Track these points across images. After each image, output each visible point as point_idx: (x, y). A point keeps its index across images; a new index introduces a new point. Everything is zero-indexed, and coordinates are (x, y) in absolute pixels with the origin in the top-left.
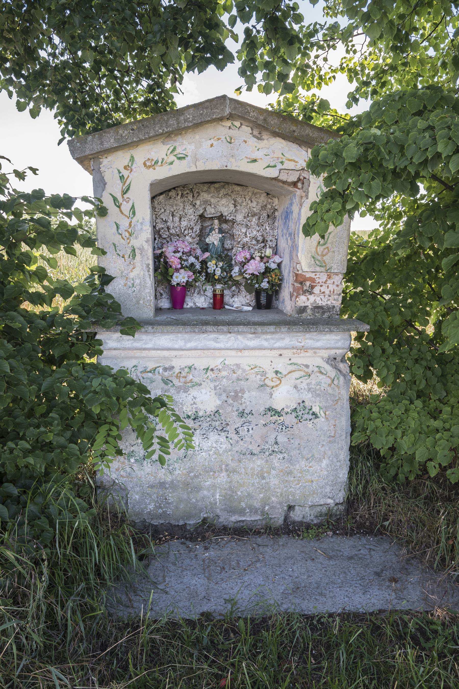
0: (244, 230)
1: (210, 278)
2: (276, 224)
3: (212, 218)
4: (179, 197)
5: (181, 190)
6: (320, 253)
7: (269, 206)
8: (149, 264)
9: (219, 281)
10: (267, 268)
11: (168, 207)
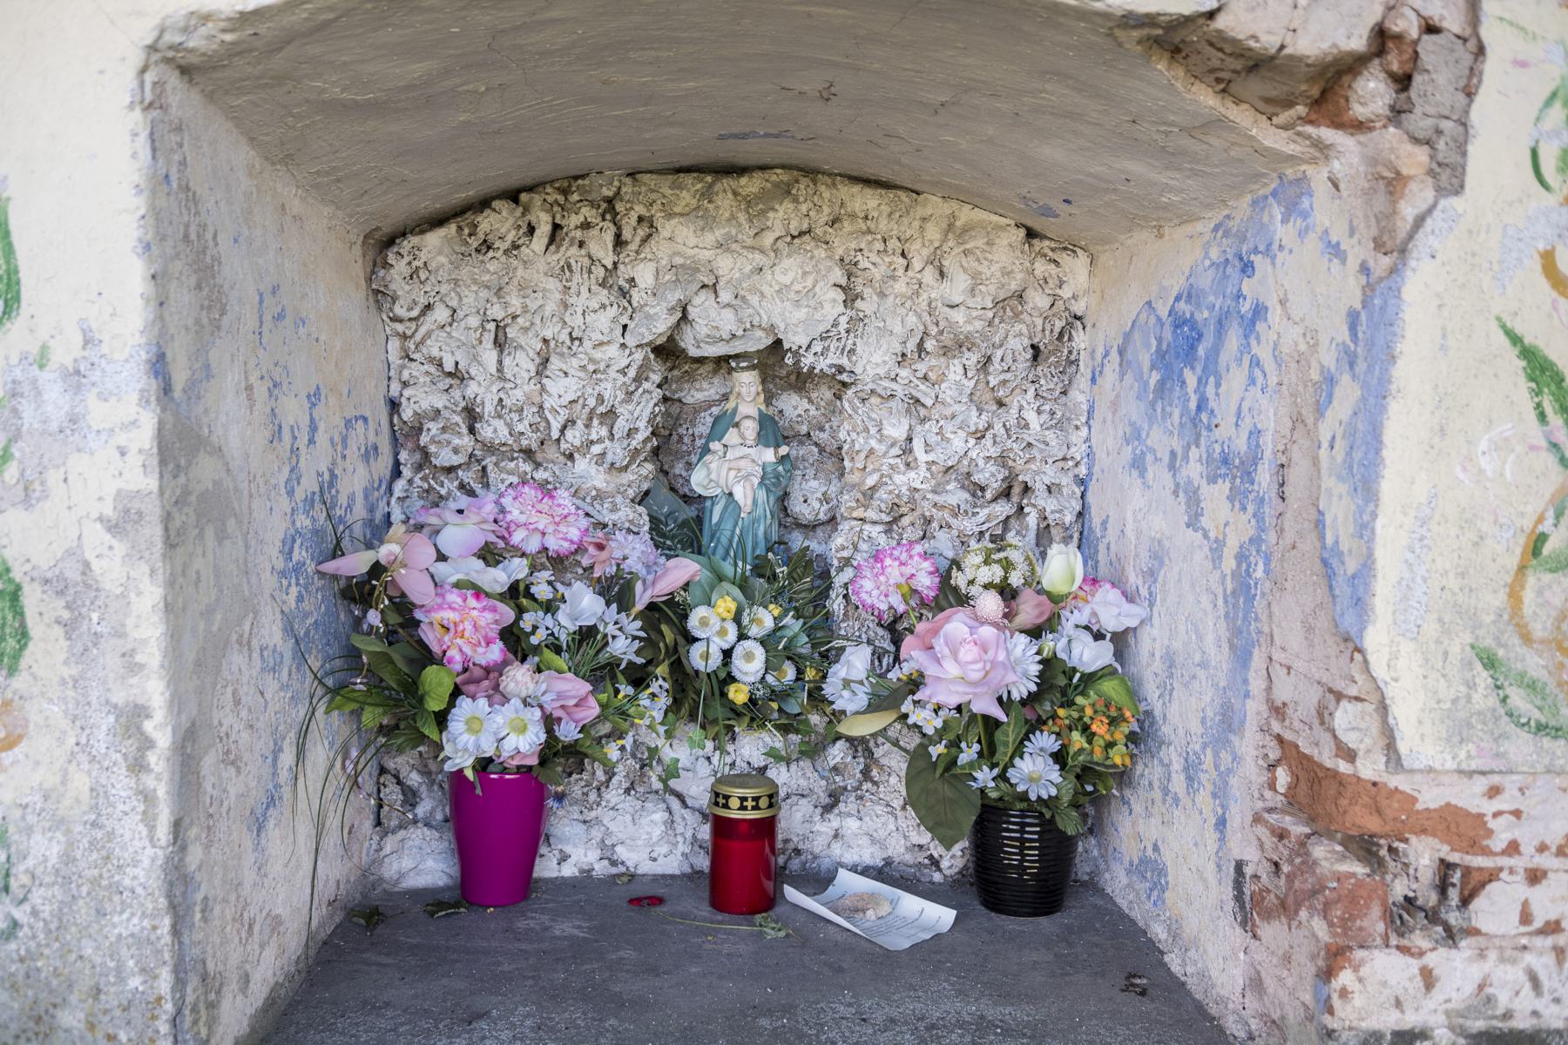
0: (896, 430)
1: (701, 700)
2: (1079, 396)
3: (723, 363)
4: (539, 241)
5: (550, 207)
6: (1539, 629)
7: (1038, 300)
8: (139, 712)
9: (754, 714)
10: (1049, 664)
11: (471, 298)
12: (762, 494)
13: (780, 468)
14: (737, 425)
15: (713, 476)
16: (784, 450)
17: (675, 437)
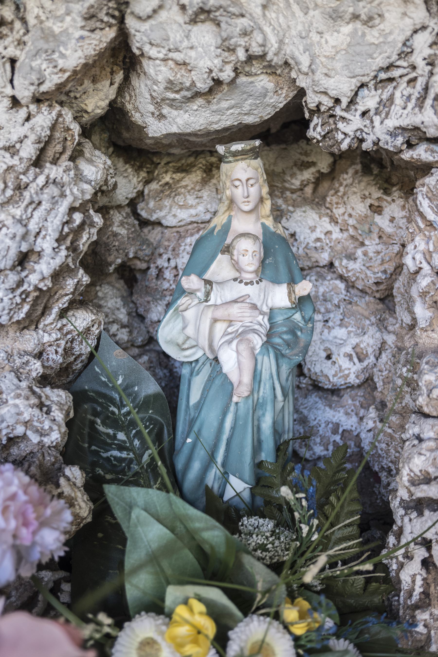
12: (268, 364)
13: (297, 317)
14: (228, 250)
15: (190, 331)
16: (304, 288)
17: (153, 272)
